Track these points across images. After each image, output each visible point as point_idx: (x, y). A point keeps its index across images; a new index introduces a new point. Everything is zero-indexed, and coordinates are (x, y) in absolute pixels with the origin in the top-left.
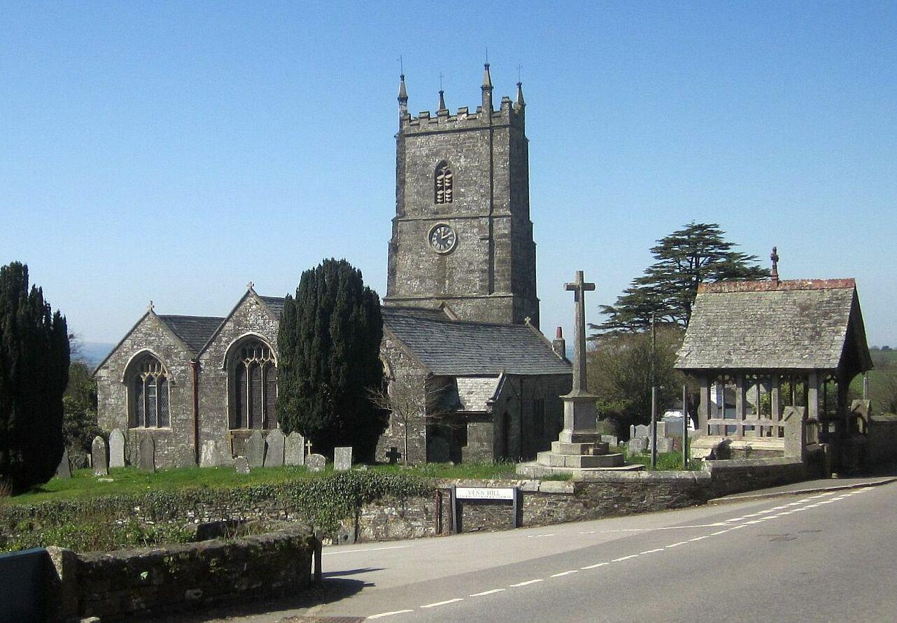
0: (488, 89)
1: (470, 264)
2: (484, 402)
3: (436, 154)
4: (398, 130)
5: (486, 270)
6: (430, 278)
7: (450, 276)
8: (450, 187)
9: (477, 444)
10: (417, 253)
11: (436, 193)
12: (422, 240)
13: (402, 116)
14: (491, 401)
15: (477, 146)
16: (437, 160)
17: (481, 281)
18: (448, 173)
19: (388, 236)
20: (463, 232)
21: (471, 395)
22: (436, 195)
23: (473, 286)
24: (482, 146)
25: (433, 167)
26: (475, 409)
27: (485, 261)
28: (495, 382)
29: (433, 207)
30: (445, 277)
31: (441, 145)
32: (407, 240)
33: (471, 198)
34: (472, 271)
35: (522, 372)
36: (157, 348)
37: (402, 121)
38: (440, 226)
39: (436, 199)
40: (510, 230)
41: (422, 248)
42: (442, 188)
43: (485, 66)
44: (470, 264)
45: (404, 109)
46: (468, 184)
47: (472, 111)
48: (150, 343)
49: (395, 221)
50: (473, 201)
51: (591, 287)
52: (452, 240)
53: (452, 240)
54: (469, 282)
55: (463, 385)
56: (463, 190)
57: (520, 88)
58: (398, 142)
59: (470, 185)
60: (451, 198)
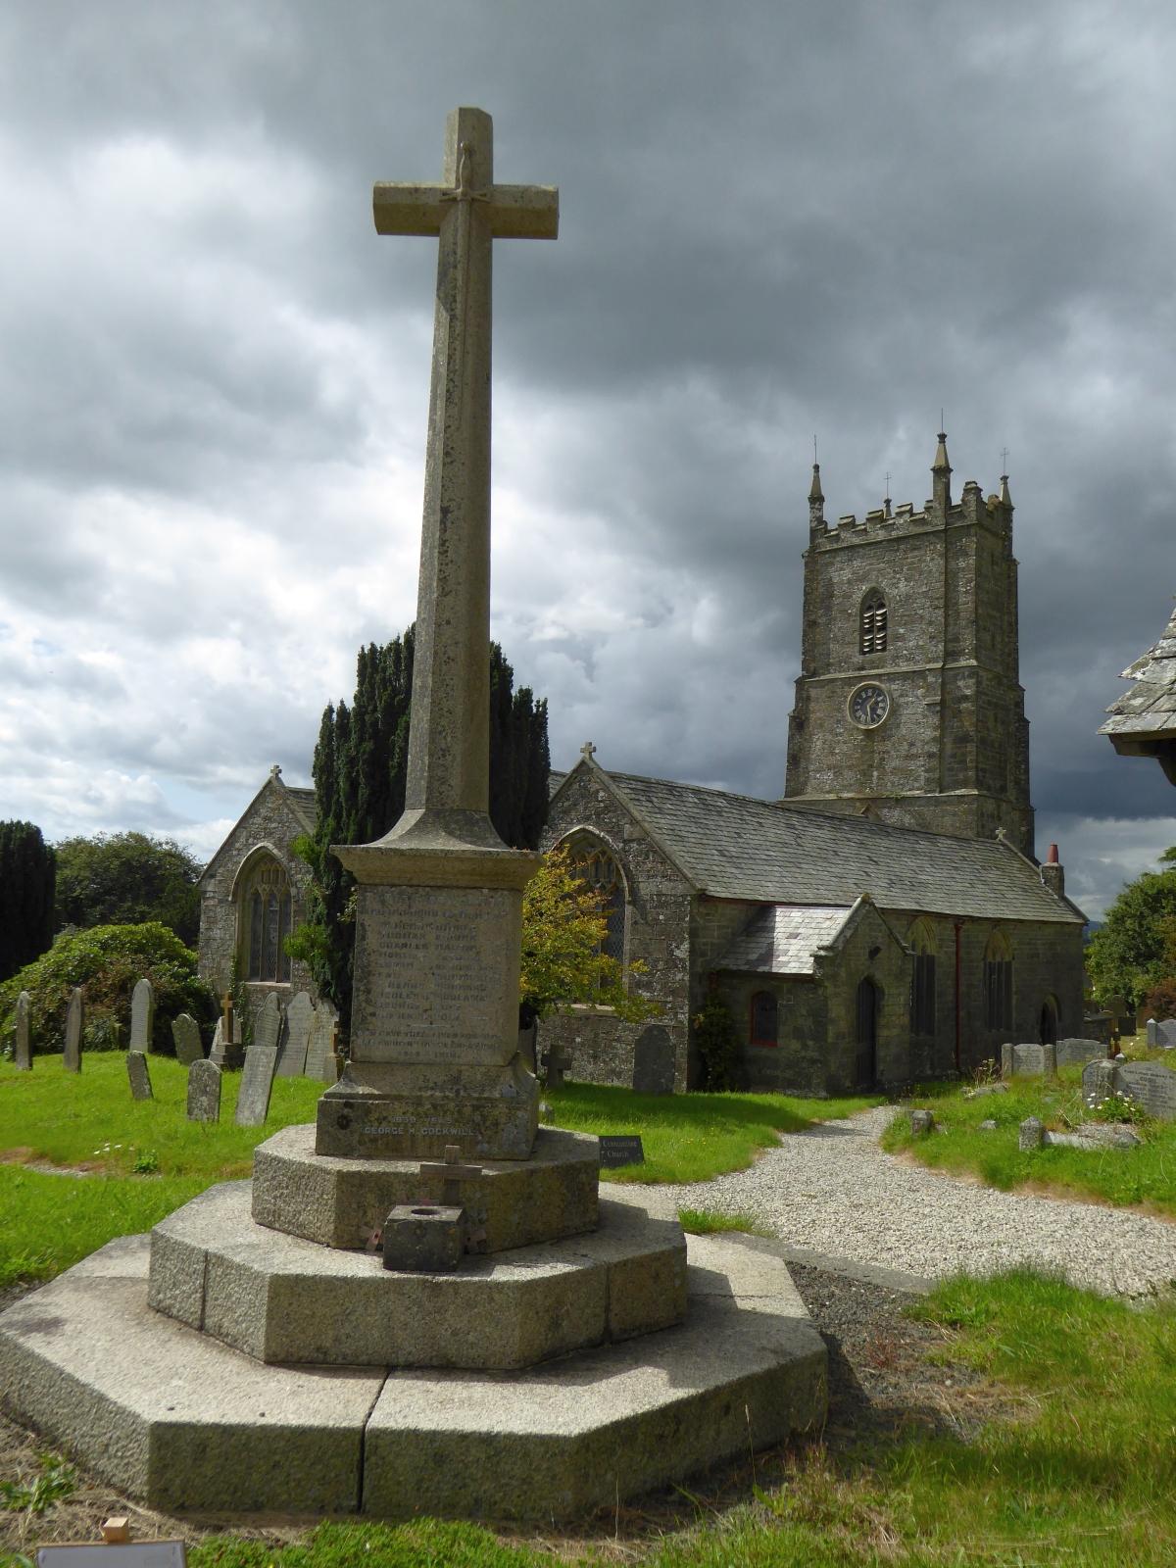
0: (942, 472)
1: (912, 745)
2: (807, 954)
3: (862, 579)
4: (807, 545)
5: (934, 753)
6: (850, 767)
7: (881, 767)
8: (883, 628)
9: (795, 1045)
10: (831, 731)
11: (861, 637)
12: (839, 710)
13: (814, 525)
14: (822, 953)
15: (925, 561)
16: (864, 588)
17: (926, 771)
18: (882, 606)
19: (790, 704)
20: (901, 696)
21: (793, 941)
22: (863, 641)
23: (916, 780)
24: (932, 559)
25: (858, 597)
26: (792, 968)
27: (934, 739)
28: (842, 916)
29: (858, 659)
30: (871, 766)
31: (871, 564)
32: (818, 711)
33: (915, 645)
34: (916, 757)
35: (959, 911)
36: (279, 844)
37: (813, 532)
38: (865, 689)
39: (862, 647)
40: (974, 688)
41: (838, 721)
42: (869, 631)
43: (939, 436)
44: (912, 745)
45: (819, 514)
46: (910, 620)
47: (919, 508)
48: (269, 834)
49: (800, 683)
50: (918, 647)
51: (536, 217)
52: (884, 709)
53: (884, 709)
54: (907, 774)
55: (785, 920)
56: (902, 631)
57: (1005, 484)
58: (806, 564)
59: (913, 622)
60: (884, 643)
